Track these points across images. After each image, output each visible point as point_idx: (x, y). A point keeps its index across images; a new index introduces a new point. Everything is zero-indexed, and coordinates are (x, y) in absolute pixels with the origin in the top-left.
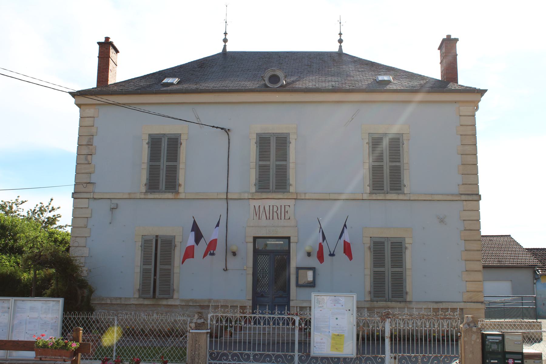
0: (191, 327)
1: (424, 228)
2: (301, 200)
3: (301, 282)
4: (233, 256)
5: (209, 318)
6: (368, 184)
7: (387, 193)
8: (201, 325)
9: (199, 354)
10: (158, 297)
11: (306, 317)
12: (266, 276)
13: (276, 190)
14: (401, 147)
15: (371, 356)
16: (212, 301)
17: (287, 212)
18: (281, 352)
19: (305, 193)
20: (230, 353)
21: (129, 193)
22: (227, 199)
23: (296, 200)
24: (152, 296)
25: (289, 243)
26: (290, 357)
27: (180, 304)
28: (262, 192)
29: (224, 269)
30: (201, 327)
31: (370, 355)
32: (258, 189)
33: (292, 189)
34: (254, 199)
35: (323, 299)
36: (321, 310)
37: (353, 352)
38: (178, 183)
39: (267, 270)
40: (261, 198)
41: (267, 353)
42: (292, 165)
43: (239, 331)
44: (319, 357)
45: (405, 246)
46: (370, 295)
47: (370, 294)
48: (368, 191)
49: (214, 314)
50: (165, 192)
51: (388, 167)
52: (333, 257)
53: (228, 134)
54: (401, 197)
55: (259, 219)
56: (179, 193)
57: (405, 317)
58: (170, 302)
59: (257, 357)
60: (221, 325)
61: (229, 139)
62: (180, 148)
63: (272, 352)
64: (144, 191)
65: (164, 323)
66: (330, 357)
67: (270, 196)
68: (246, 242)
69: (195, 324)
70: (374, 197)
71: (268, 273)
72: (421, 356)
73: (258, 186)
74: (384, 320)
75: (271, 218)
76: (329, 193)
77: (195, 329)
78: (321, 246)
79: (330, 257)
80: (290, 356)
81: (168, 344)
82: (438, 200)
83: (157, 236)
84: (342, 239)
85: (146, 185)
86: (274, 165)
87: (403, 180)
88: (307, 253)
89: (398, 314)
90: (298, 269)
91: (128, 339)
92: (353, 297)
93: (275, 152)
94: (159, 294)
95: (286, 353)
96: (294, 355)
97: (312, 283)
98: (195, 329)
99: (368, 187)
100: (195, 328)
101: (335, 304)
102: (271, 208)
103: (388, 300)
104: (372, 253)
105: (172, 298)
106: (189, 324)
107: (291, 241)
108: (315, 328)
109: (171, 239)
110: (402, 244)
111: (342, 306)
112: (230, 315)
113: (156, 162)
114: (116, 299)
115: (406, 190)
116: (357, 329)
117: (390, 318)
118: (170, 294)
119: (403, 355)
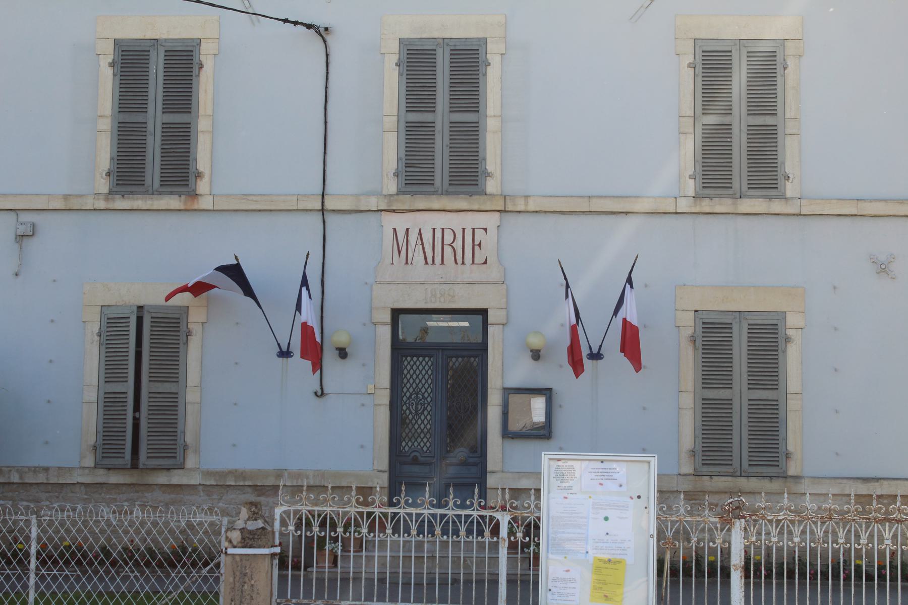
0: (230, 542)
1: (835, 288)
3: (515, 425)
4: (343, 361)
5: (277, 517)
6: (691, 171)
7: (741, 198)
8: (256, 537)
10: (144, 465)
12: (424, 411)
13: (452, 189)
14: (778, 75)
17: (479, 245)
19: (527, 197)
21: (64, 195)
22: (323, 210)
23: (503, 214)
24: (130, 462)
28: (413, 194)
29: (316, 393)
30: (258, 539)
32: (404, 185)
33: (492, 186)
34: (394, 211)
35: (572, 467)
36: (566, 498)
38: (194, 168)
39: (426, 395)
46: (693, 461)
49: (292, 508)
50: (160, 193)
51: (744, 128)
52: (599, 361)
53: (325, 41)
54: (777, 206)
55: (407, 263)
56: (196, 195)
57: (784, 517)
58: (177, 478)
60: (308, 534)
61: (327, 55)
62: (198, 76)
64: (106, 191)
68: (373, 323)
69: (242, 533)
70: (706, 206)
71: (429, 404)
73: (404, 177)
75: (438, 259)
79: (591, 361)
81: (171, 583)
82: (875, 216)
83: (140, 308)
84: (621, 314)
85: (109, 176)
88: (531, 351)
89: (764, 509)
90: (508, 392)
92: (649, 462)
94: (148, 457)
97: (542, 428)
98: (240, 545)
99: (691, 183)
100: (241, 542)
101: (602, 482)
102: (438, 234)
104: (700, 351)
105: (182, 467)
106: (226, 532)
107: (491, 319)
108: (550, 542)
111: (621, 486)
114: (36, 470)
115: (790, 189)
116: (658, 546)
117: (743, 517)
118: (175, 457)
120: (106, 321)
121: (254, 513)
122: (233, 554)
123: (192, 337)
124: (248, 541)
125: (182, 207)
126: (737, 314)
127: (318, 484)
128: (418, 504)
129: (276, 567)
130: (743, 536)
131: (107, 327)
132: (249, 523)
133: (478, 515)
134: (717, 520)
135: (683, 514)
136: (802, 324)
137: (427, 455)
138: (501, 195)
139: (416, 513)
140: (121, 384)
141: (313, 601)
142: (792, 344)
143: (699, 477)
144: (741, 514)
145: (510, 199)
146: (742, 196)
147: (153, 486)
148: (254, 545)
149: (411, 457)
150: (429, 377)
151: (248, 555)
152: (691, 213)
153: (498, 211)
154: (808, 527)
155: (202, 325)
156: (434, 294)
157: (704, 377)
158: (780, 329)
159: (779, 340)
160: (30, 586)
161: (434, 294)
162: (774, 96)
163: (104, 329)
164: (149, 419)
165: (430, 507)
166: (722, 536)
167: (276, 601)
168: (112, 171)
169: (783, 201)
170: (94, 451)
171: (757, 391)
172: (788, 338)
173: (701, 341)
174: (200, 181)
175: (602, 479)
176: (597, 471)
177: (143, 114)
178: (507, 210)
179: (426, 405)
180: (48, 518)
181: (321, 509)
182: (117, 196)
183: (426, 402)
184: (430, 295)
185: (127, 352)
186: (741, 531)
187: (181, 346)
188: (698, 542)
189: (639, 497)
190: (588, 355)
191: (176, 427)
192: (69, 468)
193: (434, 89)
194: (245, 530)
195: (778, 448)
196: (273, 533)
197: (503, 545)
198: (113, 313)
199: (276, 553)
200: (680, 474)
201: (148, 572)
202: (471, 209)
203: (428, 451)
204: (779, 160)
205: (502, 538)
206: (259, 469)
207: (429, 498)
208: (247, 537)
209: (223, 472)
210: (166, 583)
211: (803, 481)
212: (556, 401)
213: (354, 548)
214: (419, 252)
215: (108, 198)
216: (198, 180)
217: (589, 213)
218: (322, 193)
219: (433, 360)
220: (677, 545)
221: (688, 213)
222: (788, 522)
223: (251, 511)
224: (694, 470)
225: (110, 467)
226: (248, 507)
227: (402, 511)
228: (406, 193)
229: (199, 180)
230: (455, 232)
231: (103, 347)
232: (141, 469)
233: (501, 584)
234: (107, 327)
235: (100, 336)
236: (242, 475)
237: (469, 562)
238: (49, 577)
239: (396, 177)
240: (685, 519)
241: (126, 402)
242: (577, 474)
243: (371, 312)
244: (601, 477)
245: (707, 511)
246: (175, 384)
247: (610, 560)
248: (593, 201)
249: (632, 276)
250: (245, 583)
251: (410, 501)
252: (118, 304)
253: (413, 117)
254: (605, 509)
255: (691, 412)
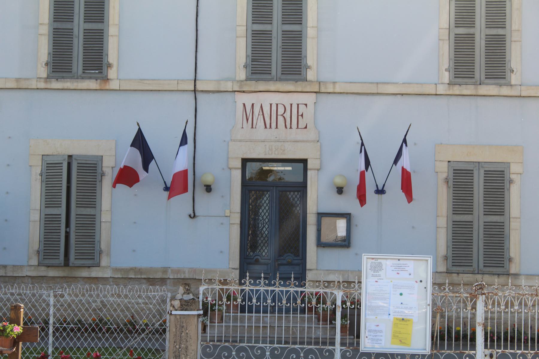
2: (326, 94)
5: (201, 292)
6: (446, 66)
7: (480, 84)
8: (189, 304)
9: (187, 348)
10: (73, 264)
11: (353, 292)
12: (263, 228)
13: (284, 77)
15: (453, 353)
16: (170, 271)
17: (302, 115)
18: (315, 345)
19: (334, 83)
20: (234, 347)
21: (16, 78)
22: (195, 91)
23: (318, 94)
25: (305, 169)
26: (327, 354)
27: (112, 276)
28: (257, 80)
29: (190, 216)
30: (190, 305)
31: (452, 351)
32: (250, 73)
33: (311, 75)
34: (244, 92)
35: (380, 263)
36: (376, 282)
37: (425, 345)
38: (106, 61)
39: (265, 217)
40: (256, 90)
41: (293, 346)
42: (311, 32)
43: (218, 323)
44: (373, 353)
45: (510, 178)
46: (446, 263)
47: (446, 261)
48: (446, 80)
49: (210, 287)
50: (83, 78)
51: (483, 37)
52: (383, 195)
54: (505, 91)
55: (252, 127)
56: (108, 79)
57: (508, 294)
58: (95, 273)
59: (276, 352)
60: (220, 302)
63: (299, 345)
64: (45, 75)
65: (87, 310)
66: (389, 353)
67: (272, 86)
68: (229, 168)
69: (180, 301)
70: (457, 90)
71: (266, 223)
72: (531, 354)
73: (251, 69)
74: (476, 296)
75: (274, 125)
76: (377, 83)
77: (179, 309)
78: (362, 175)
79: (377, 195)
80: (328, 351)
81: (136, 332)
83: (70, 157)
84: (400, 164)
85: (47, 65)
86: (280, 33)
87: (510, 61)
88: (337, 188)
89: (497, 289)
90: (320, 215)
91: (72, 325)
92: (427, 260)
93: (280, 8)
94: (76, 259)
95: (322, 347)
96: (334, 350)
98: (179, 309)
99: (447, 74)
100: (180, 307)
101: (398, 272)
103: (476, 272)
104: (452, 189)
105: (98, 265)
106: (171, 300)
107: (309, 166)
108: (367, 308)
109: (95, 163)
110: (504, 174)
111: (410, 274)
112: (234, 287)
113: (64, 23)
115: (514, 79)
116: (433, 311)
117: (484, 294)
118: (94, 259)
119: (503, 352)
120: (46, 165)
121: (187, 290)
122: (176, 314)
123: (105, 177)
124: (184, 306)
125: (98, 88)
126: (477, 164)
127: (191, 277)
128: (287, 284)
129: (200, 323)
130: (484, 305)
131: (47, 170)
132: (185, 296)
133: (323, 292)
134: (468, 295)
135: (448, 292)
136: (521, 171)
137: (265, 258)
138: (317, 81)
139: (285, 291)
140: (56, 208)
141: (223, 343)
142: (514, 185)
143: (450, 274)
144: (483, 292)
145: (323, 84)
146: (481, 83)
147: (78, 278)
148: (188, 309)
149: (254, 259)
150: (267, 205)
151: (185, 315)
152: (446, 95)
153: (315, 92)
154: (523, 300)
155: (112, 169)
156: (271, 148)
157: (454, 206)
158: (506, 174)
159: (505, 182)
160: (50, 334)
161: (271, 148)
162: (504, 15)
163: (44, 171)
164: (76, 232)
165: (294, 287)
166: (471, 305)
167: (200, 343)
168: (49, 62)
169: (509, 87)
170: (38, 254)
171: (490, 216)
172: (511, 180)
173: (452, 182)
174: (110, 70)
175: (399, 270)
176: (396, 265)
177: (71, 23)
178: (321, 91)
179: (265, 224)
180: (60, 293)
181: (228, 288)
182: (53, 80)
183: (265, 222)
184: (268, 149)
185: (61, 187)
186: (483, 302)
187: (98, 183)
188: (457, 309)
189: (421, 281)
190: (375, 191)
191: (94, 238)
192: (21, 266)
193: (271, 8)
194: (183, 300)
195: (504, 255)
196: (199, 302)
197: (338, 310)
198: (51, 160)
199: (200, 314)
200: (437, 272)
201: (122, 325)
202: (296, 91)
203: (266, 256)
204: (507, 59)
205: (338, 305)
206: (151, 267)
207: (293, 282)
208: (183, 304)
209: (127, 269)
210: (133, 332)
211: (520, 277)
212: (354, 222)
213: (217, 320)
214: (261, 120)
215: (47, 81)
216: (109, 69)
217: (377, 94)
218: (194, 79)
219: (270, 193)
220: (444, 311)
221: (444, 95)
222: (511, 297)
223: (186, 289)
224: (447, 269)
225: (48, 265)
226: (184, 286)
227: (277, 289)
228: (252, 79)
229: (109, 69)
230: (286, 106)
231: (44, 184)
232: (71, 266)
233: (337, 333)
234: (47, 170)
235: (42, 176)
236: (138, 271)
237: (295, 330)
238: (61, 328)
239: (245, 68)
240: (449, 295)
241: (60, 221)
242: (384, 267)
243: (228, 160)
244: (398, 269)
245: (462, 290)
246: (93, 209)
247: (403, 319)
248: (380, 86)
249: (407, 138)
250: (182, 332)
251: (282, 283)
252: (54, 154)
253: (257, 27)
254: (401, 288)
255: (445, 230)
